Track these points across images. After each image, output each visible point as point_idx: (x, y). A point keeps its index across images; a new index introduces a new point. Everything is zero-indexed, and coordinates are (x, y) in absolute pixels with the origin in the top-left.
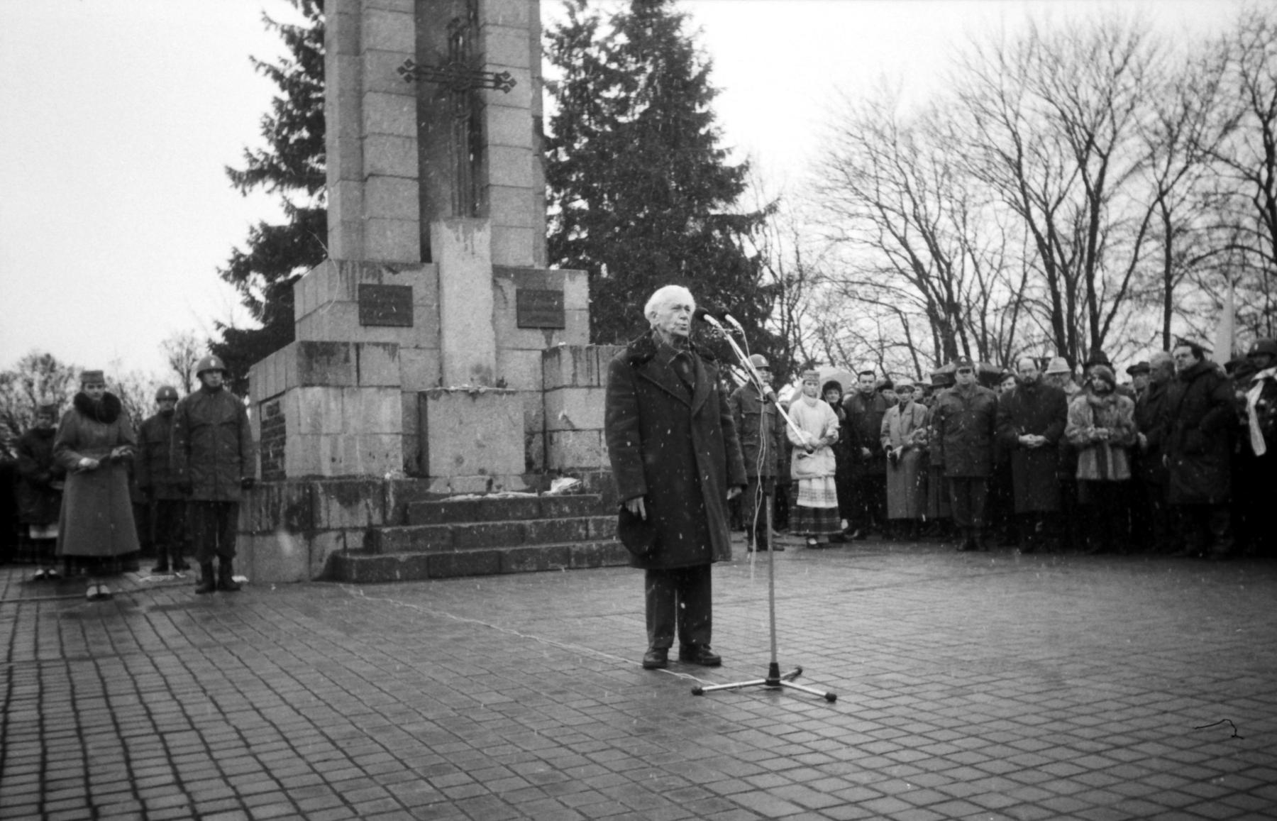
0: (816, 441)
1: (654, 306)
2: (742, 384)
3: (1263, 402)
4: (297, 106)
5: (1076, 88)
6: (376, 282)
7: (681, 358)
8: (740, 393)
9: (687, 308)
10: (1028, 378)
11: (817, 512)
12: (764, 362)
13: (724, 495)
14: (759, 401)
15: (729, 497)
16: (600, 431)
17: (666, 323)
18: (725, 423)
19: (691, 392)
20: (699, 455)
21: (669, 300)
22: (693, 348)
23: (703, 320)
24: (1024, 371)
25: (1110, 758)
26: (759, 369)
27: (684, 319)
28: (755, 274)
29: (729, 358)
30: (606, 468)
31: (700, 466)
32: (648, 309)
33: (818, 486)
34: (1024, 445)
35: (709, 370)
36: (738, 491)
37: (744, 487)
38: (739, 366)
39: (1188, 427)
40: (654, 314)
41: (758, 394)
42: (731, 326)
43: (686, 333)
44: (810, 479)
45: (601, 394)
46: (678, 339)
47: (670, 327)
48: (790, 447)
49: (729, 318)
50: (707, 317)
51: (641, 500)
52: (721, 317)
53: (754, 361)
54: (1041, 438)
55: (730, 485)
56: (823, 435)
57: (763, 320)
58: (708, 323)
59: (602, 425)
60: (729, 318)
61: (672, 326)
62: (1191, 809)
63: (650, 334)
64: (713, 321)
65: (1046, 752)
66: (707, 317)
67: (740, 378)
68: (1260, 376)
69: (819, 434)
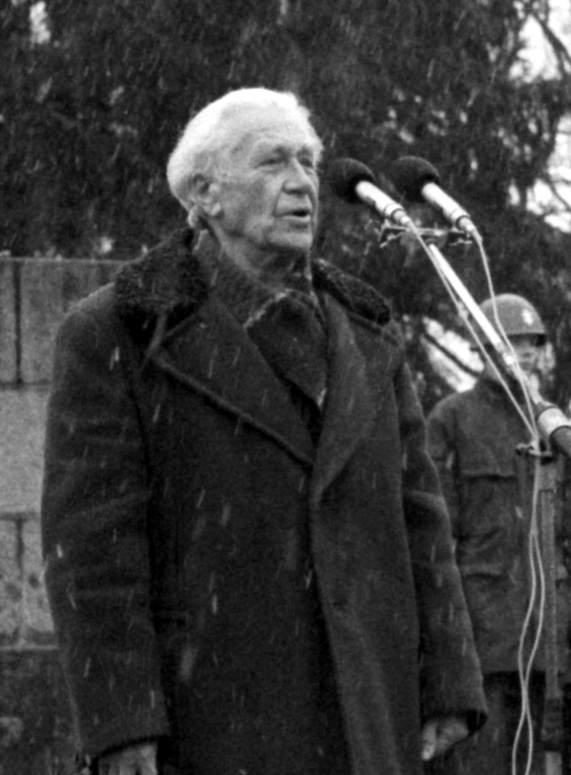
1: (200, 157)
2: (465, 384)
7: (289, 317)
8: (455, 414)
9: (304, 157)
12: (529, 317)
13: (412, 750)
14: (526, 455)
15: (427, 754)
16: (19, 521)
17: (243, 213)
18: (418, 517)
19: (315, 419)
20: (334, 615)
21: (247, 138)
22: (321, 282)
23: (354, 198)
26: (516, 339)
27: (299, 192)
28: (499, 41)
29: (419, 295)
30: (36, 636)
31: (337, 646)
32: (178, 166)
35: (369, 352)
36: (457, 729)
37: (474, 720)
38: (452, 323)
40: (199, 182)
41: (527, 439)
42: (437, 216)
43: (306, 239)
45: (36, 405)
46: (283, 259)
47: (259, 223)
49: (433, 192)
50: (366, 189)
51: (148, 753)
52: (409, 193)
53: (509, 317)
55: (433, 713)
57: (525, 184)
58: (371, 208)
59: (31, 499)
60: (433, 192)
61: (264, 220)
63: (189, 238)
64: (384, 202)
66: (366, 189)
67: (456, 361)
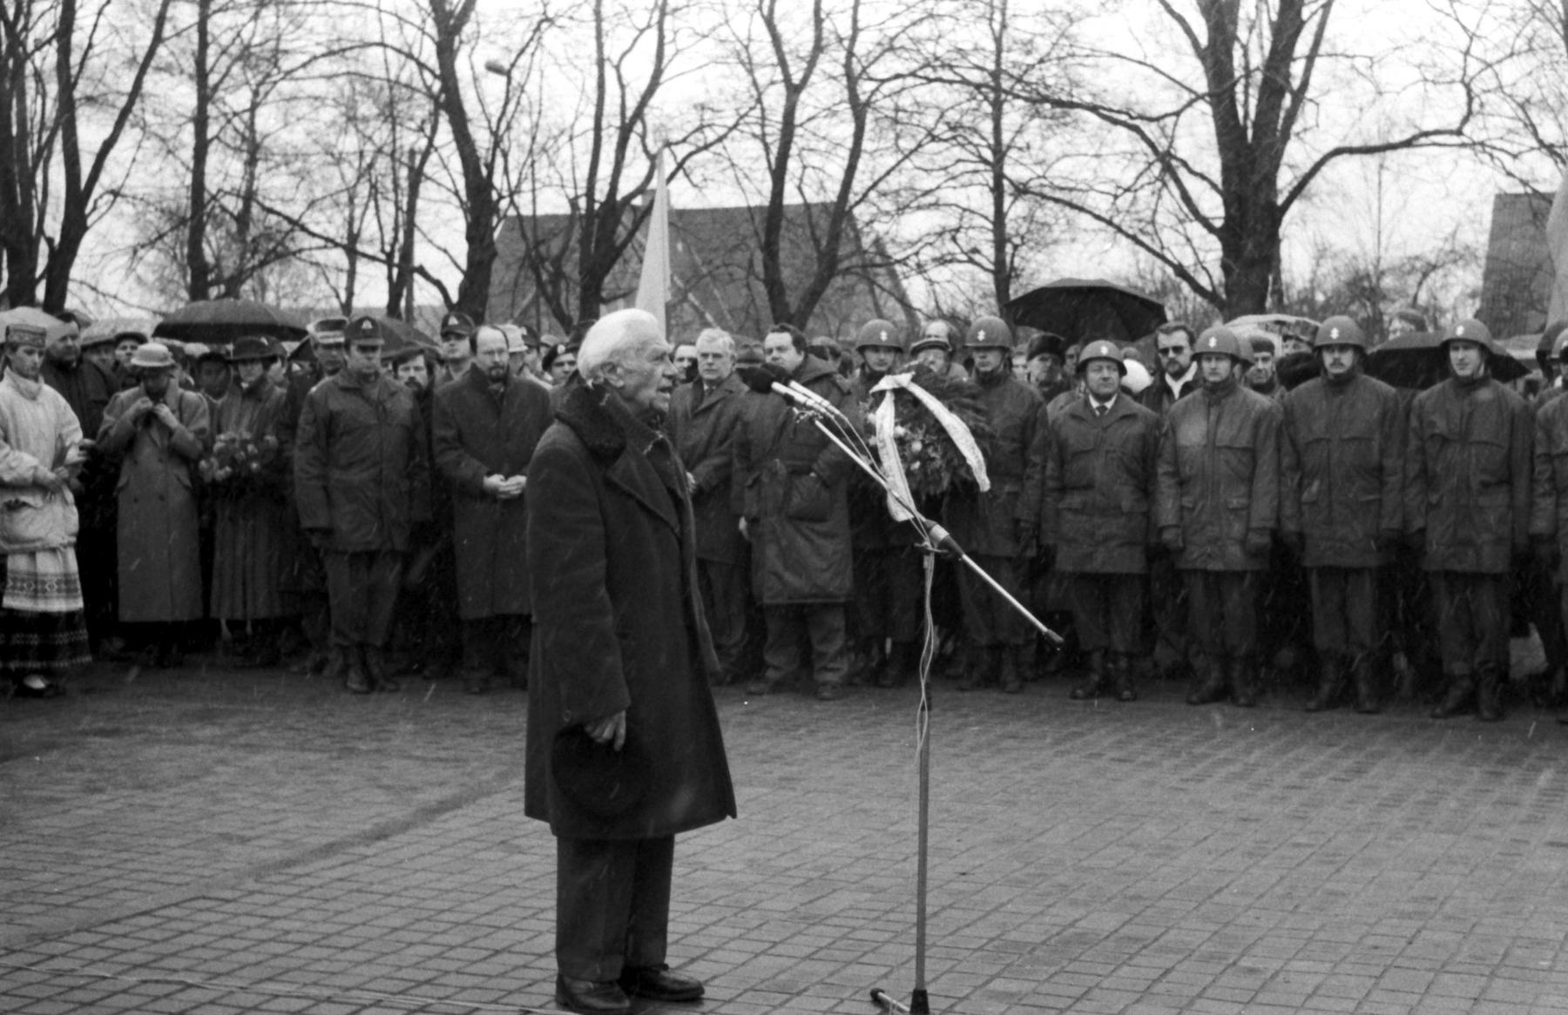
0: (47, 474)
3: (901, 431)
4: (1228, 292)
5: (1492, 156)
6: (1368, 586)
10: (496, 366)
11: (47, 621)
24: (491, 353)
25: (108, 948)
33: (47, 565)
34: (492, 495)
39: (796, 472)
44: (32, 554)
48: (760, 610)
54: (522, 479)
56: (59, 458)
62: (28, 1001)
65: (35, 959)
68: (886, 383)
69: (49, 460)
